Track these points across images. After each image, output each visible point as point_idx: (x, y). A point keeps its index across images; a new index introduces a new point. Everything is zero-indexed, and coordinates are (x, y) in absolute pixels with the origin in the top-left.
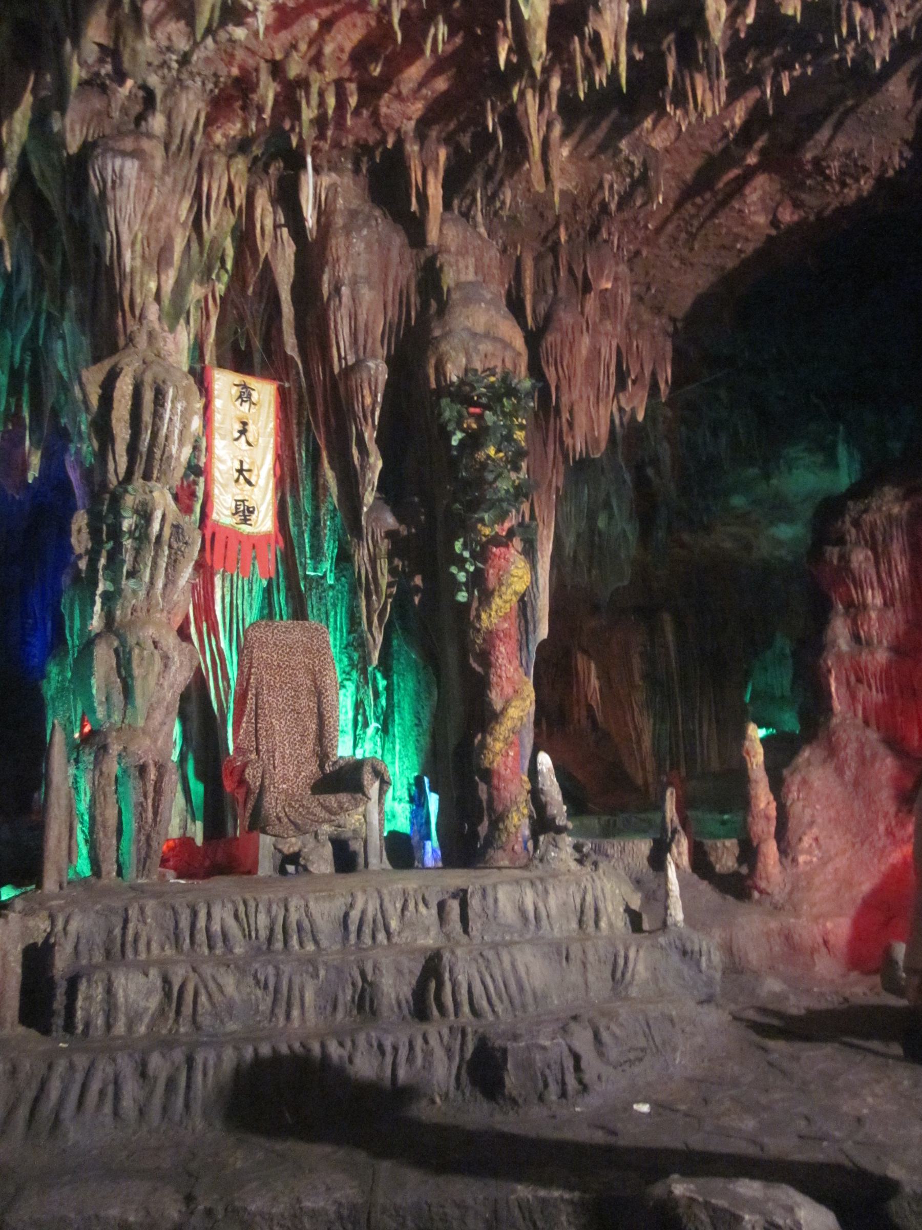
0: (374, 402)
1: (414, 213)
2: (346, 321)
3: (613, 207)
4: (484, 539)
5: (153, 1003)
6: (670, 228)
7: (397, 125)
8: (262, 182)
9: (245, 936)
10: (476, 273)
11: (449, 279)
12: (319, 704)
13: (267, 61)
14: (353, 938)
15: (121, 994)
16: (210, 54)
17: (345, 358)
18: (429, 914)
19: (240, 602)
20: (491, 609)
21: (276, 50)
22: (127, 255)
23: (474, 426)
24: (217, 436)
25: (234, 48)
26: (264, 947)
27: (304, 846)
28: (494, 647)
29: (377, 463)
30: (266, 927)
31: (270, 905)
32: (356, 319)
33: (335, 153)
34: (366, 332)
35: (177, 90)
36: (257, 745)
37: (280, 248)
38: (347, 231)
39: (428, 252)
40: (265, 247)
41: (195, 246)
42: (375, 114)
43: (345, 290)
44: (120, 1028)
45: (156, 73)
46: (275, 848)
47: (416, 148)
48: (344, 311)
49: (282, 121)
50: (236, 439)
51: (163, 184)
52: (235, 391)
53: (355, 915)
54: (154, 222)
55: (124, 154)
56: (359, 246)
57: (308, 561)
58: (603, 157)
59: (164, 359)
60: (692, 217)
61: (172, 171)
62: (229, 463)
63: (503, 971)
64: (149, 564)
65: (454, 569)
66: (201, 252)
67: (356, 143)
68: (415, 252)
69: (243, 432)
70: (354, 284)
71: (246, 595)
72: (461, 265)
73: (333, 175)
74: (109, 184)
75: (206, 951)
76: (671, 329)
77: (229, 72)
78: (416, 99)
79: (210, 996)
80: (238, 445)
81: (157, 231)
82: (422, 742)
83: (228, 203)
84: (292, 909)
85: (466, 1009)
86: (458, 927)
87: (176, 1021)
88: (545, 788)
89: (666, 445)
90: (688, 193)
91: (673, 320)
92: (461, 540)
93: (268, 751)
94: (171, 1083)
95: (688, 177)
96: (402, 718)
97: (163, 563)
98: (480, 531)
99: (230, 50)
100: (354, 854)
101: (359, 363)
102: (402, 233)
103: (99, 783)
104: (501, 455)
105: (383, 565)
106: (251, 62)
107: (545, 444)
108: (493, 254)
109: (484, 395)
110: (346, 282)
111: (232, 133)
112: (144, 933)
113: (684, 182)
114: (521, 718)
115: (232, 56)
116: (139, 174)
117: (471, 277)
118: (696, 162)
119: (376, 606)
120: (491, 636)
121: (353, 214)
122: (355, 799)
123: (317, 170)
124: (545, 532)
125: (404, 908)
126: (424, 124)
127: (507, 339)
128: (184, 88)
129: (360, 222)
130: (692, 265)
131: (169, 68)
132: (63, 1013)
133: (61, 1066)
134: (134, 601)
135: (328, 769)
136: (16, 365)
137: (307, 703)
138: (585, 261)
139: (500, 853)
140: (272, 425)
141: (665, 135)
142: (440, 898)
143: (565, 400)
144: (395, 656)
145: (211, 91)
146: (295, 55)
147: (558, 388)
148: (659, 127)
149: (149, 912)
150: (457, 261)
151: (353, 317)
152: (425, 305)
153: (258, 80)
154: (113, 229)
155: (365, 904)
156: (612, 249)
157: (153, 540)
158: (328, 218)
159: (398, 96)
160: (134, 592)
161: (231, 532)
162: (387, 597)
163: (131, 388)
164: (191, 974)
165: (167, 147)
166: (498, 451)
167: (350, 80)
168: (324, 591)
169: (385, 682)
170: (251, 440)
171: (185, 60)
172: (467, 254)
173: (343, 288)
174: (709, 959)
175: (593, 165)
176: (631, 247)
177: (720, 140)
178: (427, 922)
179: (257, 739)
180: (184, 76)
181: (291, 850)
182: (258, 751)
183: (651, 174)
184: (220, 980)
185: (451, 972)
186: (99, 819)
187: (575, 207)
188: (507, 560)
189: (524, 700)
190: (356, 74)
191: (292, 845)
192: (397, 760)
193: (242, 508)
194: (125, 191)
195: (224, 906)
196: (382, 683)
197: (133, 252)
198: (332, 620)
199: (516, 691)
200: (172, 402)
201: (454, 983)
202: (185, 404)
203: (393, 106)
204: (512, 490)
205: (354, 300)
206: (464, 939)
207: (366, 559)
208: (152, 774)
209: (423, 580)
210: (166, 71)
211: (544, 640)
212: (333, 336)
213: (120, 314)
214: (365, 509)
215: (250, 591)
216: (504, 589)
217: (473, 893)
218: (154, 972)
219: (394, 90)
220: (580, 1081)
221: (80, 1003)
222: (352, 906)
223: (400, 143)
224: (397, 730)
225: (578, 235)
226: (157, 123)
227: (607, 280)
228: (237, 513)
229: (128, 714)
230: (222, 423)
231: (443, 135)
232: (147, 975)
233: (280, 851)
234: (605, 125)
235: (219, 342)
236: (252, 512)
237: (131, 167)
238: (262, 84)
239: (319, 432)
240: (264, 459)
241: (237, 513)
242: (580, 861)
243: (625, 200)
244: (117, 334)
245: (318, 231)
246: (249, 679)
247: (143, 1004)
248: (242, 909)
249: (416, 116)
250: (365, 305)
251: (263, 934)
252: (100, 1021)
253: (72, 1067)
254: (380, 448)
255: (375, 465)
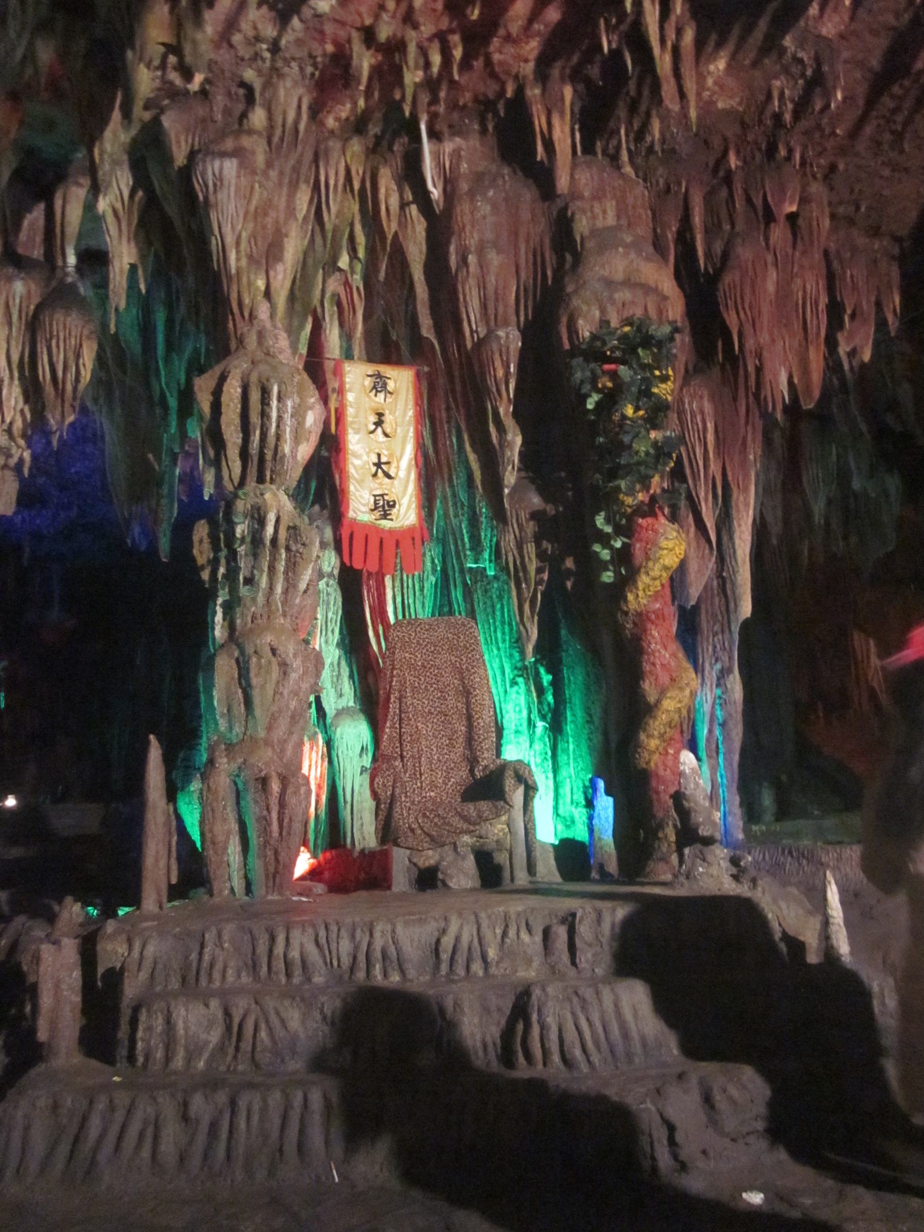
0: (507, 374)
1: (542, 162)
2: (475, 292)
3: (788, 117)
4: (629, 510)
5: (215, 1037)
6: (868, 130)
7: (514, 71)
8: (386, 162)
9: (326, 963)
10: (618, 217)
11: (582, 226)
12: (468, 704)
13: (358, 29)
14: (444, 968)
15: (180, 1024)
16: (301, 35)
17: (477, 332)
18: (532, 942)
19: (411, 601)
20: (637, 588)
21: (365, 16)
22: (232, 256)
23: (610, 384)
24: (350, 431)
25: (322, 23)
26: (346, 977)
27: (442, 859)
28: (645, 630)
29: (516, 440)
30: (349, 954)
31: (354, 931)
32: (484, 288)
33: (455, 115)
34: (497, 300)
35: (275, 80)
36: (402, 751)
37: (409, 226)
38: (471, 195)
39: (560, 203)
40: (391, 228)
41: (319, 240)
42: (488, 63)
43: (472, 259)
44: (179, 1062)
45: (250, 67)
46: (410, 861)
47: (537, 91)
48: (472, 282)
49: (392, 91)
50: (372, 432)
51: (267, 178)
52: (368, 382)
53: (447, 942)
54: (259, 219)
55: (223, 155)
56: (484, 208)
57: (468, 553)
58: (767, 61)
59: (273, 357)
60: (894, 111)
61: (276, 163)
62: (365, 458)
63: (602, 1013)
64: (266, 569)
65: (597, 548)
66: (325, 245)
67: (476, 100)
68: (547, 204)
69: (379, 423)
70: (481, 252)
71: (417, 594)
72: (597, 210)
73: (458, 139)
74: (211, 188)
75: (283, 980)
76: (896, 251)
77: (324, 50)
78: (528, 37)
79: (270, 1029)
80: (382, 437)
81: (264, 227)
82: (595, 741)
83: (348, 188)
84: (377, 935)
85: (556, 1058)
86: (566, 958)
87: (235, 1057)
88: (687, 792)
89: (906, 386)
90: (880, 84)
91: (897, 239)
92: (603, 514)
93: (413, 757)
94: (214, 1128)
95: (875, 63)
96: (574, 715)
97: (281, 567)
98: (623, 502)
99: (318, 26)
100: (498, 869)
101: (490, 332)
102: (534, 187)
103: (208, 798)
104: (641, 413)
105: (530, 549)
106: (342, 34)
107: (735, 399)
108: (639, 193)
109: (617, 348)
110: (473, 249)
111: (344, 115)
112: (221, 959)
113: (871, 70)
114: (679, 710)
115: (322, 32)
116: (238, 172)
117: (611, 220)
118: (883, 42)
119: (527, 595)
120: (642, 618)
121: (478, 177)
122: (496, 807)
123: (434, 135)
124: (741, 498)
125: (505, 934)
126: (544, 62)
127: (652, 283)
128: (281, 76)
129: (487, 183)
130: (906, 170)
131: (263, 60)
132: (126, 1043)
133: (101, 1105)
134: (253, 609)
135: (478, 774)
136: (183, 387)
137: (454, 703)
138: (764, 187)
139: (661, 866)
140: (411, 413)
141: (836, 19)
142: (547, 922)
143: (750, 344)
144: (564, 647)
145: (313, 75)
146: (385, 17)
147: (741, 334)
148: (828, 11)
149: (226, 937)
150: (592, 207)
151: (482, 285)
152: (561, 260)
153: (351, 49)
154: (216, 232)
155: (460, 930)
156: (795, 167)
157: (268, 543)
158: (453, 186)
159: (508, 38)
160: (254, 600)
161: (369, 531)
162: (538, 583)
163: (239, 390)
164: (253, 1006)
165: (269, 143)
166: (637, 409)
167: (451, 31)
168: (489, 583)
169: (550, 677)
170: (388, 431)
171: (275, 48)
172: (604, 200)
173: (470, 257)
174: (883, 1004)
175: (757, 73)
176: (822, 161)
177: (906, 10)
178: (529, 951)
179: (401, 745)
180: (279, 64)
181: (427, 864)
182: (402, 757)
183: (826, 68)
184: (283, 1015)
185: (539, 1011)
186: (208, 835)
187: (744, 125)
188: (656, 532)
189: (681, 689)
190: (455, 24)
191: (428, 858)
192: (571, 761)
193: (381, 503)
194: (225, 191)
195: (304, 930)
196: (546, 678)
197: (238, 252)
198: (498, 613)
199: (673, 680)
200: (280, 399)
201: (543, 1027)
202: (297, 400)
203: (505, 51)
204: (652, 451)
205: (481, 267)
206: (572, 972)
207: (512, 544)
208: (275, 786)
209: (576, 562)
210: (260, 62)
211: (746, 620)
212: (463, 310)
213: (230, 317)
214: (506, 491)
215: (422, 589)
216: (650, 564)
217: (582, 918)
218: (214, 1003)
219: (502, 32)
220: (676, 1157)
221: (140, 1034)
222: (444, 931)
223: (520, 91)
224: (569, 728)
225: (754, 159)
226: (258, 117)
227: (791, 204)
228: (376, 508)
229: (250, 725)
230: (356, 417)
231: (568, 71)
232: (207, 1005)
233: (415, 865)
234: (763, 25)
235: (367, 333)
236: (394, 506)
237: (230, 167)
238: (355, 55)
239: (460, 415)
240: (403, 449)
241: (376, 508)
242: (736, 878)
243: (801, 107)
244: (228, 339)
245: (445, 201)
246: (392, 681)
247: (203, 1036)
248: (322, 933)
249: (533, 56)
250: (493, 269)
251: (346, 961)
252: (159, 1054)
253: (112, 1108)
254: (518, 422)
255: (514, 442)
